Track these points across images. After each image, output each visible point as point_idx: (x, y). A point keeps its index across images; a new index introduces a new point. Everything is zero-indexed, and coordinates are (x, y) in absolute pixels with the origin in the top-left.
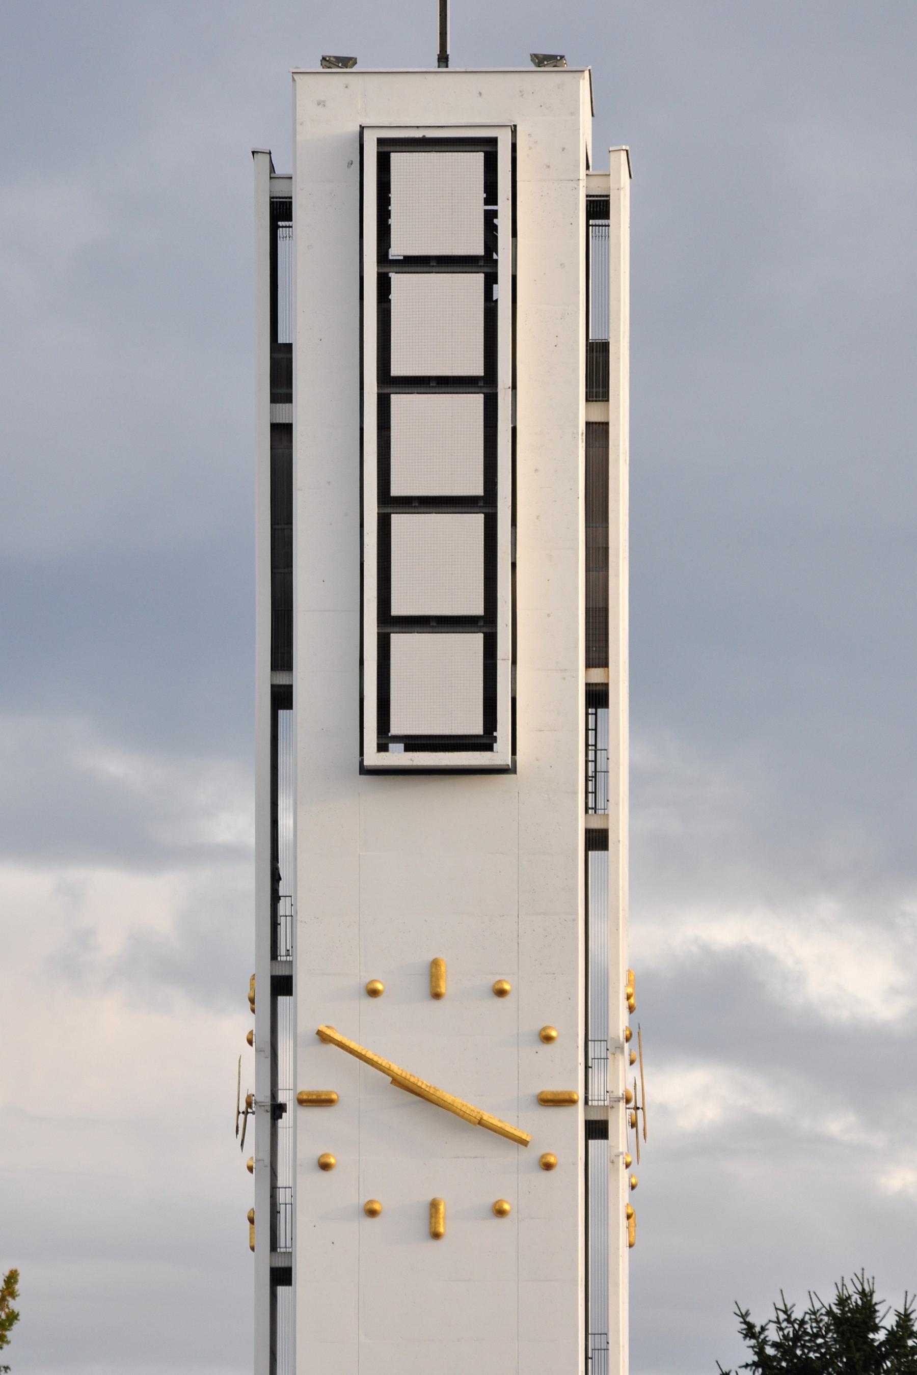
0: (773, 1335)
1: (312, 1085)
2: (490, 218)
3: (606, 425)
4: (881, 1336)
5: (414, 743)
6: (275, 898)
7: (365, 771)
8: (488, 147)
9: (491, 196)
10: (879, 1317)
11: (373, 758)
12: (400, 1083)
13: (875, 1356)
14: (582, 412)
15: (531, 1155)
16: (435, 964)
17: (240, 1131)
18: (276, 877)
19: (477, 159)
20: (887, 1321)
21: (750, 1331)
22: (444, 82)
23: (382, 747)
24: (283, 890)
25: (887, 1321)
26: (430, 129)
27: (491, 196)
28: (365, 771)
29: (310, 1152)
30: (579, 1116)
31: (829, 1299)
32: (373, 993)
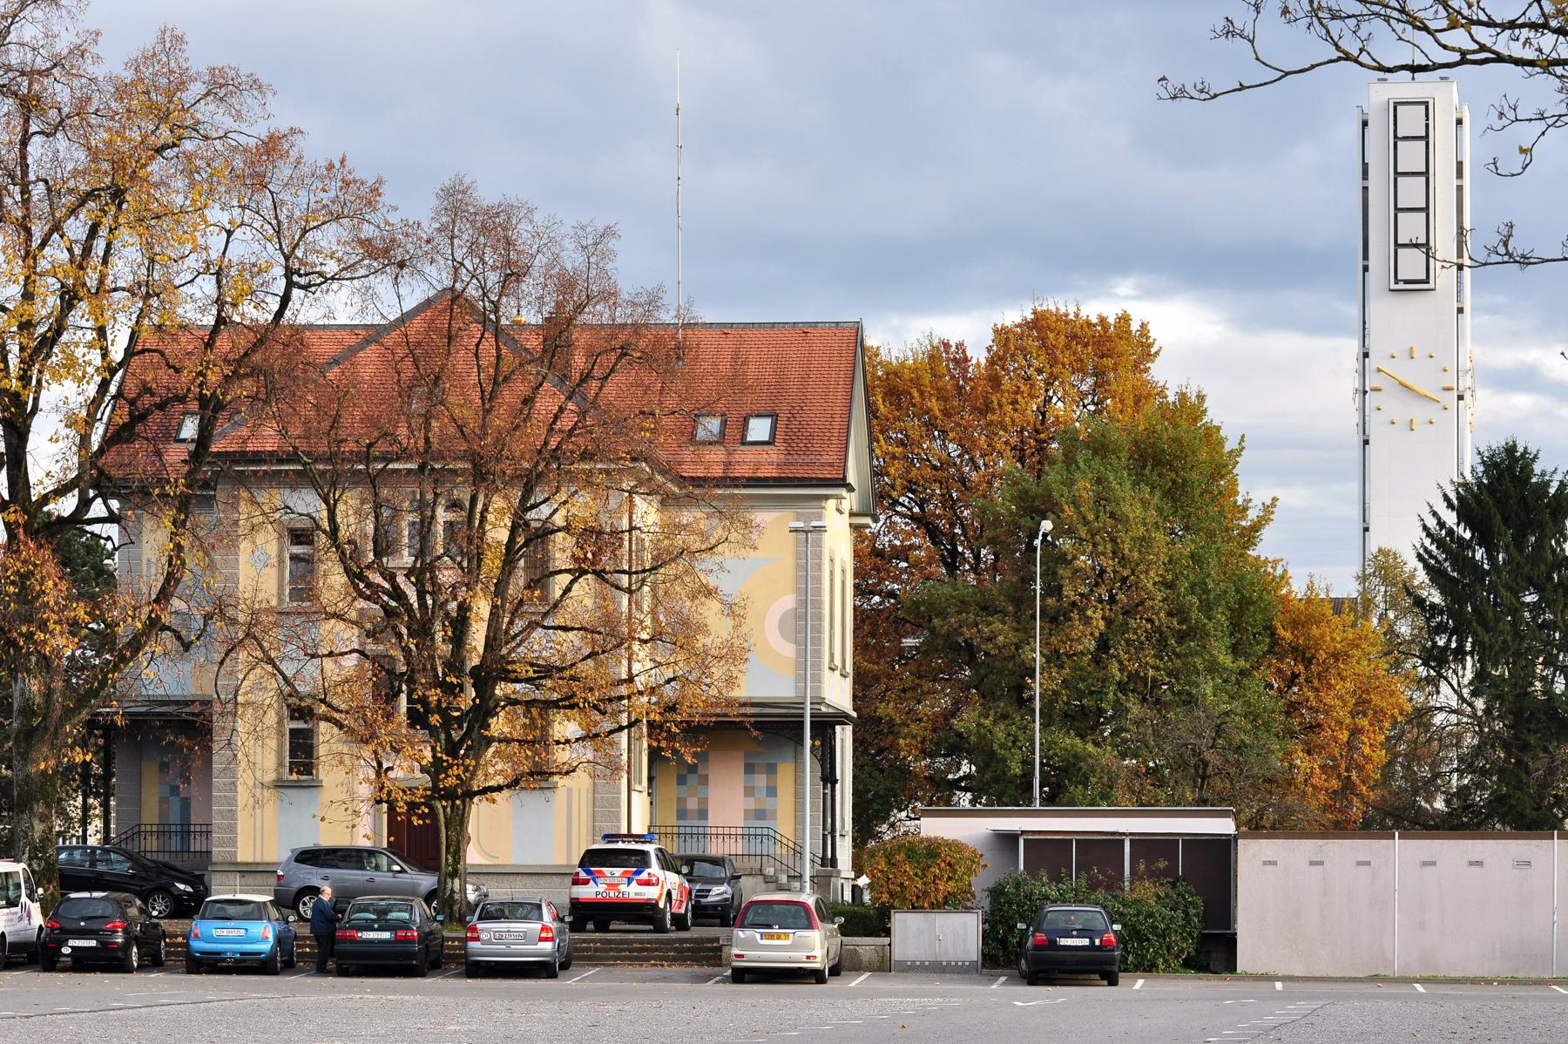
0: (1486, 454)
1: (1374, 385)
2: (1427, 125)
3: (1462, 186)
4: (1518, 454)
5: (1406, 282)
6: (1364, 329)
7: (1390, 290)
8: (1426, 104)
9: (1427, 116)
10: (238, 116)
11: (1393, 286)
12: (1401, 384)
13: (1516, 460)
14: (1455, 182)
15: (1440, 406)
16: (1412, 348)
17: (1354, 400)
18: (1364, 322)
19: (1423, 107)
20: (1520, 449)
21: (1479, 453)
22: (1413, 85)
23: (1396, 283)
24: (1367, 326)
25: (1520, 449)
26: (543, 881)
27: (1427, 116)
28: (1390, 290)
29: (1374, 405)
30: (1455, 394)
31: (1503, 443)
32: (1393, 357)
